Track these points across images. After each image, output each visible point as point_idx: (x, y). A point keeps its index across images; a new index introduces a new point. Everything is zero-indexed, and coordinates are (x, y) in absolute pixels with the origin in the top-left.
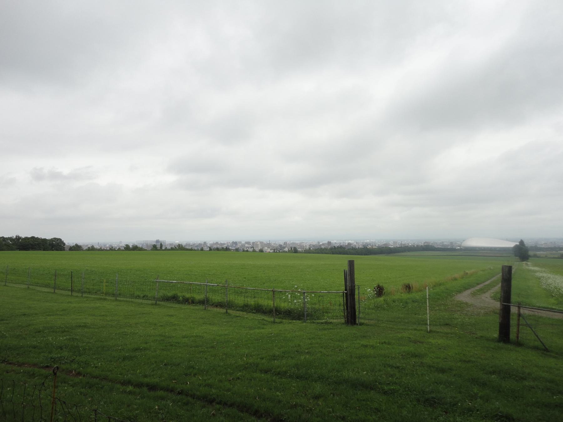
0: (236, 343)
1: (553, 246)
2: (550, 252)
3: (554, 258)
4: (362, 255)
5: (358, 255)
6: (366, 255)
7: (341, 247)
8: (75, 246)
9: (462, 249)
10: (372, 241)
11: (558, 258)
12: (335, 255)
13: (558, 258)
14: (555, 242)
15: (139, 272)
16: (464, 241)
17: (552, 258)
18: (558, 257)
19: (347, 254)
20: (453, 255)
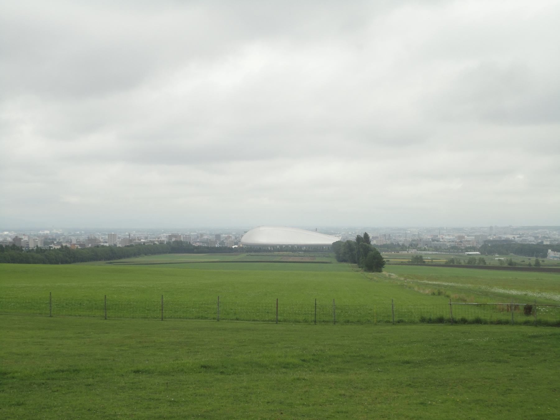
0: (240, 355)
1: (389, 242)
2: (387, 253)
3: (402, 264)
4: (57, 263)
5: (51, 263)
6: (67, 262)
7: (64, 249)
8: (64, 247)
9: (242, 248)
10: (55, 231)
11: (409, 264)
12: (32, 264)
13: (409, 264)
14: (389, 235)
15: (331, 400)
16: (246, 232)
17: (399, 264)
18: (408, 262)
19: (28, 262)
20: (267, 262)
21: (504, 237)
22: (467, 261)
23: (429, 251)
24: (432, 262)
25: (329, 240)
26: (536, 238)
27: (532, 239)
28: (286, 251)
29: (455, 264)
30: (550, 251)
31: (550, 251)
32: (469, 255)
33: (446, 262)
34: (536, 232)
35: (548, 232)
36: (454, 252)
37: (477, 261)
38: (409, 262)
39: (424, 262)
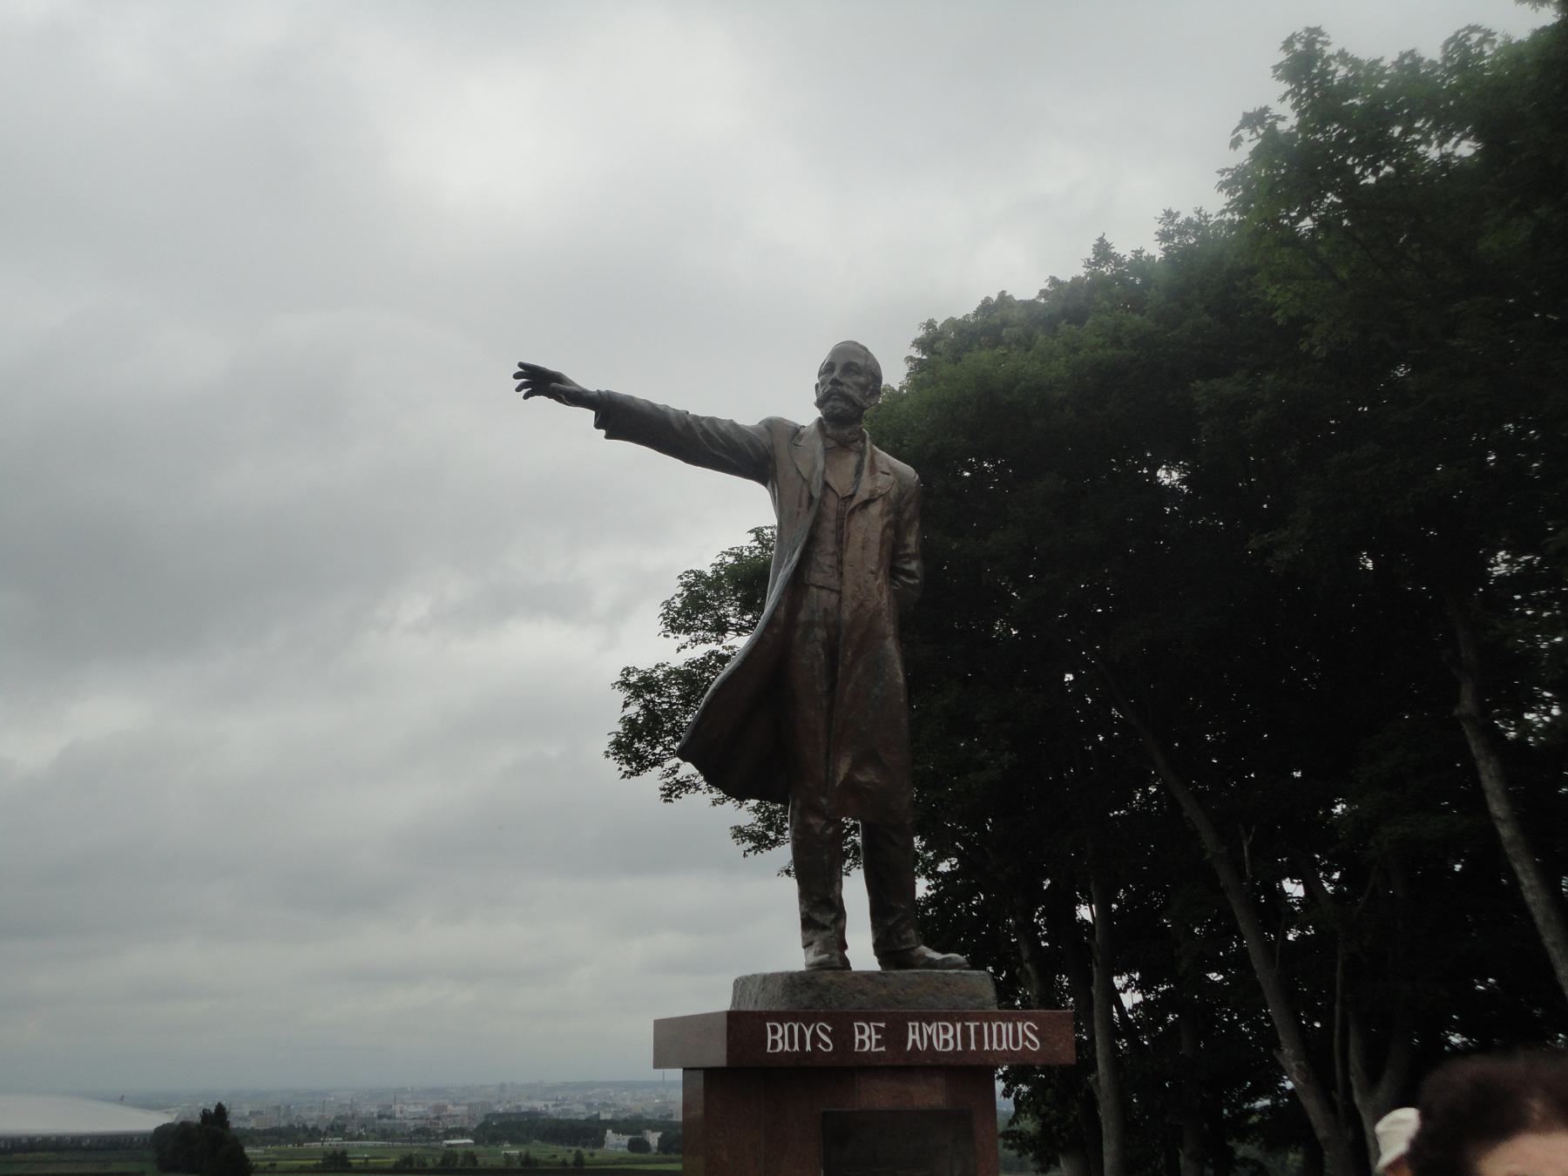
21: (526, 1105)
22: (439, 1160)
23: (367, 1138)
24: (366, 1163)
25: (146, 1122)
26: (589, 1106)
27: (582, 1108)
28: (43, 1150)
29: (415, 1166)
30: (609, 1132)
31: (609, 1132)
32: (450, 1145)
33: (397, 1164)
34: (590, 1093)
35: (612, 1094)
36: (420, 1141)
37: (460, 1159)
38: (316, 1166)
39: (350, 1165)
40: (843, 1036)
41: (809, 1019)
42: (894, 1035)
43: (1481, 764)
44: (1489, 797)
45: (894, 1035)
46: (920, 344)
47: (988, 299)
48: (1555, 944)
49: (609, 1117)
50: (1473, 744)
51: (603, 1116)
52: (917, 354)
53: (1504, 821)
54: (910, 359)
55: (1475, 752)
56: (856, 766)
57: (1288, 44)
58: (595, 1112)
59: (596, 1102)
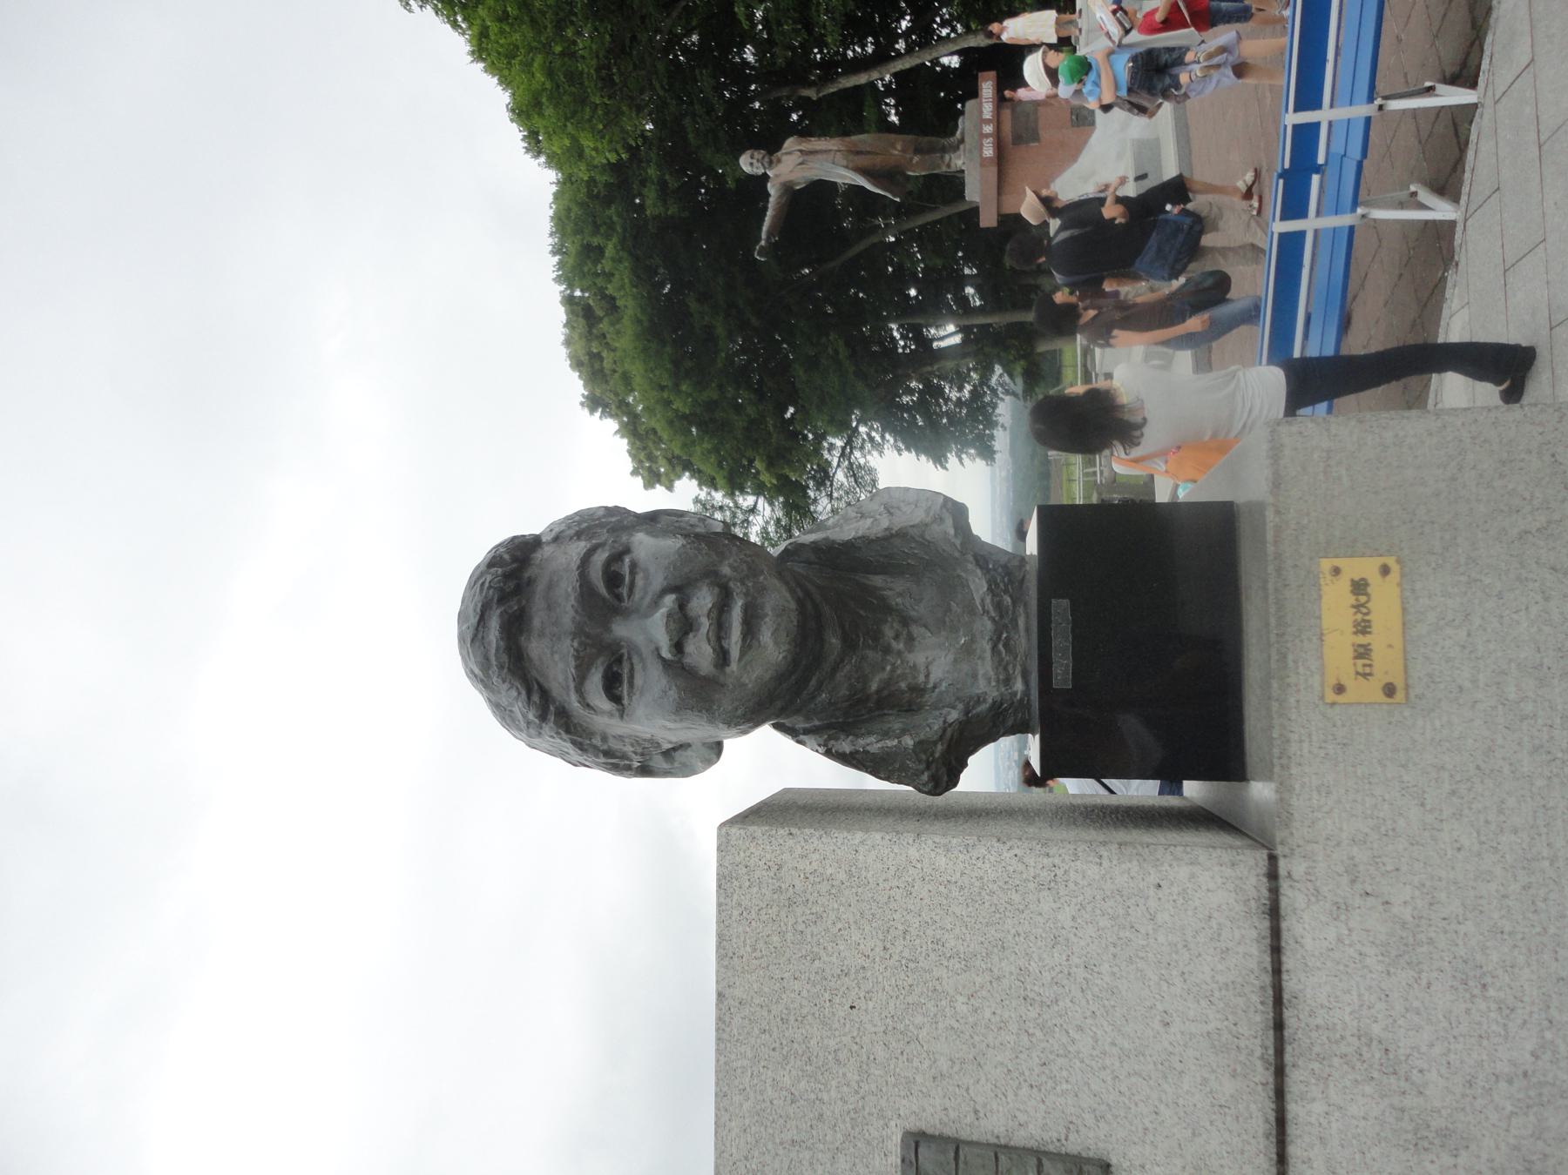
26: (1010, 768)
27: (1011, 773)
40: (987, 136)
41: (982, 145)
42: (988, 122)
43: (841, 86)
44: (857, 83)
45: (988, 122)
46: (592, 411)
47: (571, 366)
48: (930, 54)
49: (1016, 754)
50: (832, 90)
51: (1016, 757)
52: (598, 414)
53: (870, 76)
54: (601, 418)
55: (835, 90)
56: (896, 149)
57: (512, 120)
58: (1014, 764)
59: (1007, 763)
